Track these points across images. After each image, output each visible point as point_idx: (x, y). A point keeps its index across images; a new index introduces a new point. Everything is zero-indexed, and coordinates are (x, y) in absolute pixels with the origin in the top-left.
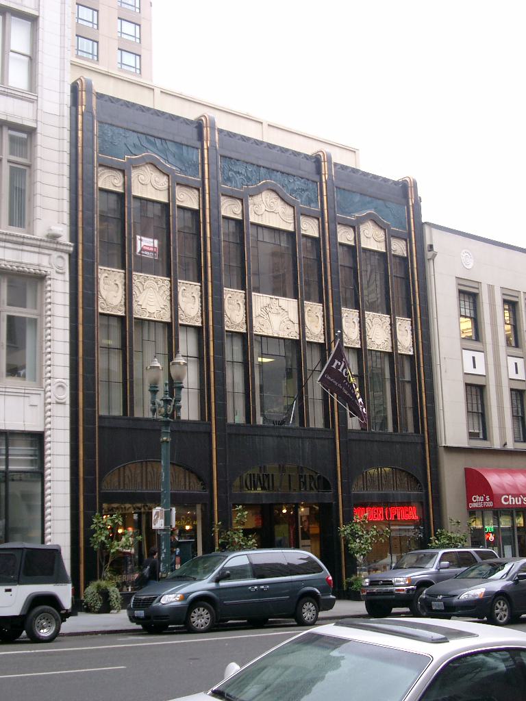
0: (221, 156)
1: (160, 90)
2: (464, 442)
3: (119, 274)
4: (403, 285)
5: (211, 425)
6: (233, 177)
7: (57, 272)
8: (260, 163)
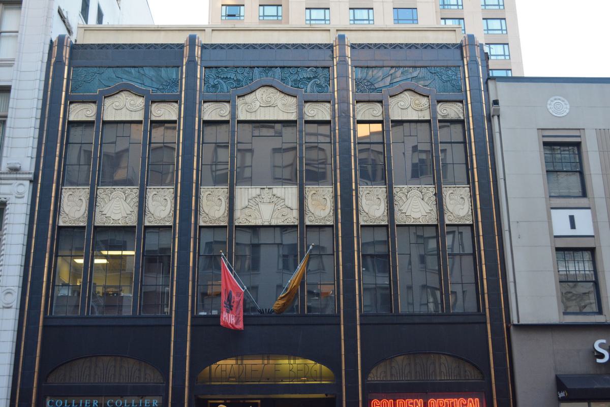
0: (205, 68)
1: (83, 29)
2: (553, 315)
3: (381, 189)
4: (464, 148)
5: (485, 315)
6: (219, 83)
7: (16, 197)
8: (253, 64)
